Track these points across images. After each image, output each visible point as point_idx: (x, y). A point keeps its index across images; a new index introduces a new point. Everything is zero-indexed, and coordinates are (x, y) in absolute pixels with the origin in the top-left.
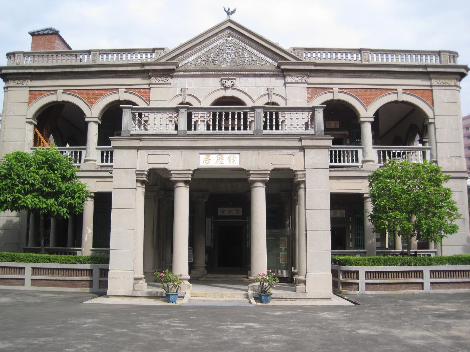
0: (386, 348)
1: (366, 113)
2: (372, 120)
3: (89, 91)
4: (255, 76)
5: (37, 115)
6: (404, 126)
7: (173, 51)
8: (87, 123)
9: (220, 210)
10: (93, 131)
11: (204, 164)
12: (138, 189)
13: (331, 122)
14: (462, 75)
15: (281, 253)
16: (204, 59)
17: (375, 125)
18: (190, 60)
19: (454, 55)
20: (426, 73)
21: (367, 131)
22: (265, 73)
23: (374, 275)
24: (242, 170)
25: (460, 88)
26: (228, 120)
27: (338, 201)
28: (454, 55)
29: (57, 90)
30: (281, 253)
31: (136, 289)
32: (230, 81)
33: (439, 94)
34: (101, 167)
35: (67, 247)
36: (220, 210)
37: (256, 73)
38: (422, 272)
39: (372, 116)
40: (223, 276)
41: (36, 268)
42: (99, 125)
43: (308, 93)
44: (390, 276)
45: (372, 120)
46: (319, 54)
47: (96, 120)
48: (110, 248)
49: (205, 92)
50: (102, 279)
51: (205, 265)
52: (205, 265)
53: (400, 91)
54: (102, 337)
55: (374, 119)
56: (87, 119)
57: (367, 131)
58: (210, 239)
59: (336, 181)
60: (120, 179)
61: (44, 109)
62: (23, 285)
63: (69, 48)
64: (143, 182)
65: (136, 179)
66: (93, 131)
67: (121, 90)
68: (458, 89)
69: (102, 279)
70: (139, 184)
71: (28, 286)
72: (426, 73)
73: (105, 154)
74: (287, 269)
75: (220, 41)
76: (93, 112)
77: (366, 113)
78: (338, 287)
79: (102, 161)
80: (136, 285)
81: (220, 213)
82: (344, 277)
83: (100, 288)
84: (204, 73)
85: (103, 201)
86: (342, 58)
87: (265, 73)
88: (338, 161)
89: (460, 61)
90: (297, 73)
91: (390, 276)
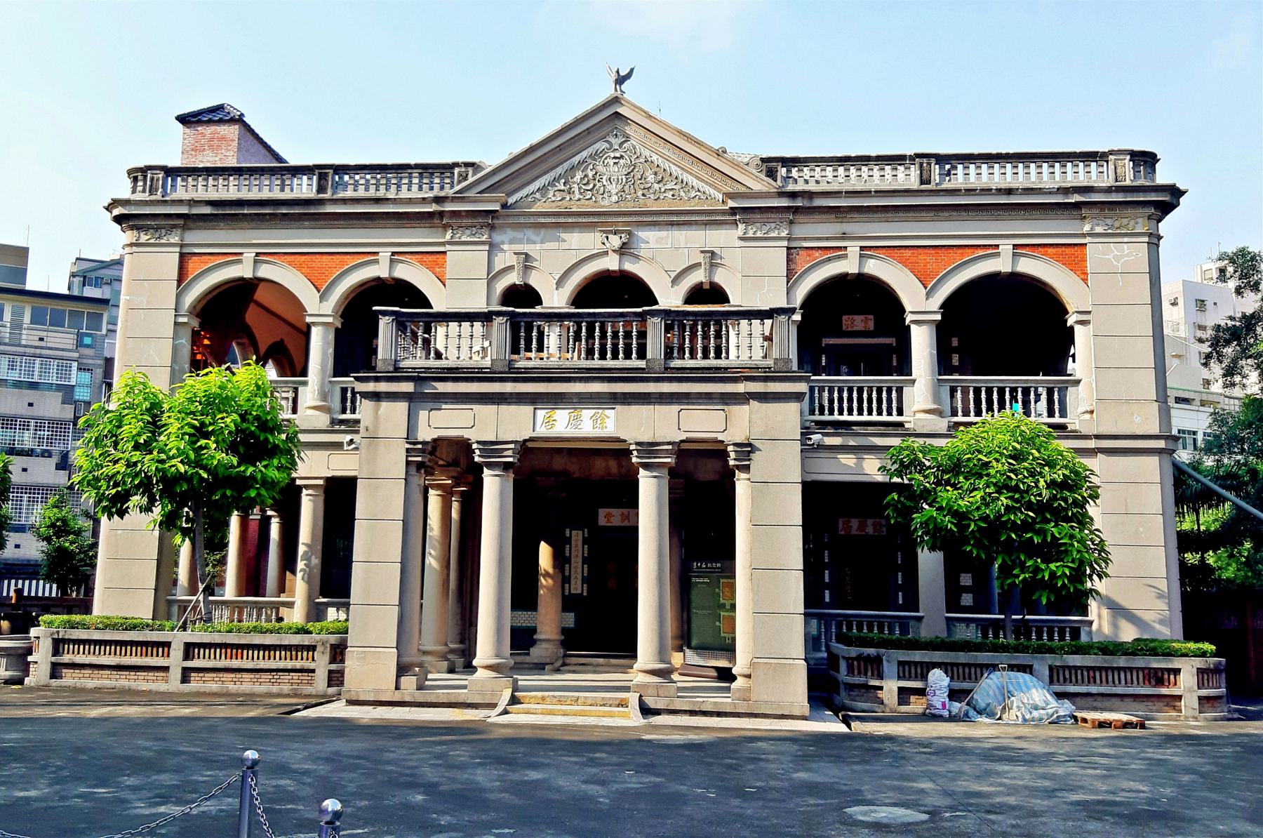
0: (73, 626)
1: (921, 302)
2: (939, 317)
3: (314, 257)
5: (199, 308)
9: (602, 512)
10: (320, 348)
13: (855, 317)
14: (1165, 208)
17: (943, 332)
21: (922, 344)
27: (823, 503)
28: (1146, 160)
29: (241, 254)
35: (944, 364)
36: (602, 512)
38: (622, 644)
39: (936, 309)
41: (909, 663)
45: (939, 317)
47: (330, 320)
48: (348, 596)
49: (557, 269)
50: (334, 667)
57: (922, 344)
58: (580, 577)
60: (367, 449)
61: (211, 296)
66: (320, 348)
71: (173, 682)
81: (602, 521)
83: (329, 686)
84: (562, 220)
85: (340, 495)
86: (877, 179)
89: (1163, 176)
90: (765, 216)
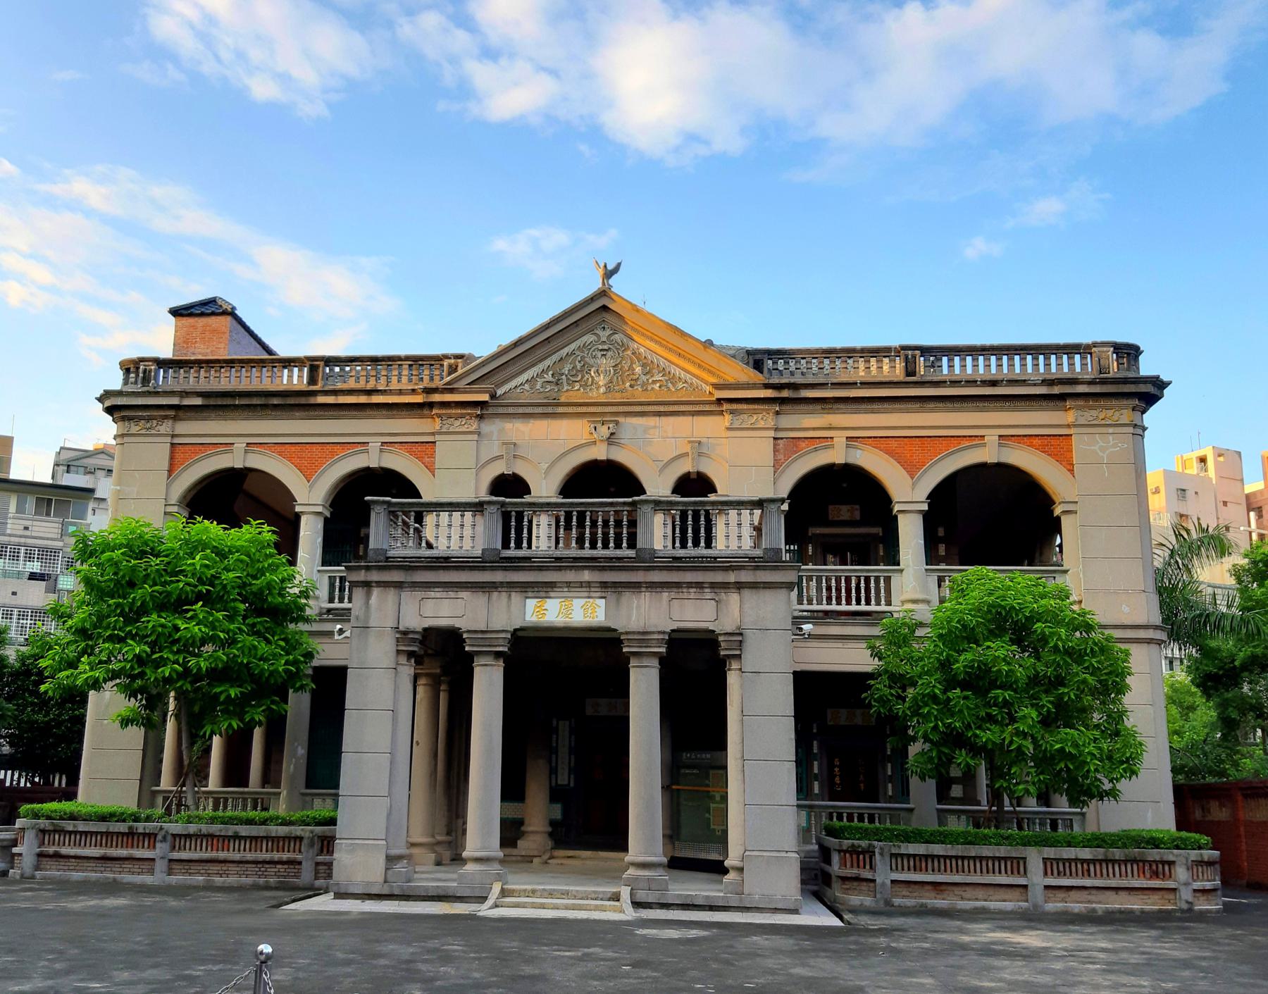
1: (909, 493)
2: (925, 507)
4: (659, 414)
6: (998, 517)
7: (484, 364)
8: (297, 517)
11: (534, 619)
12: (400, 668)
15: (712, 805)
16: (549, 377)
17: (931, 521)
18: (517, 385)
19: (1129, 352)
20: (1058, 394)
21: (911, 534)
22: (682, 408)
23: (912, 863)
24: (609, 630)
25: (1144, 429)
26: (584, 527)
28: (1129, 352)
30: (712, 805)
31: (389, 879)
32: (605, 427)
33: (1086, 446)
34: (329, 611)
37: (662, 409)
40: (588, 853)
42: (326, 519)
43: (775, 451)
44: (1105, 871)
46: (803, 362)
47: (320, 509)
49: (547, 452)
50: (321, 858)
51: (550, 829)
52: (550, 829)
53: (990, 439)
54: (310, 964)
55: (929, 505)
56: (298, 509)
57: (911, 534)
59: (840, 645)
62: (151, 872)
63: (269, 351)
64: (410, 655)
65: (394, 649)
67: (374, 445)
68: (1140, 432)
69: (321, 858)
70: (403, 659)
72: (1058, 394)
73: (337, 584)
74: (697, 844)
75: (585, 339)
76: (311, 496)
77: (909, 493)
78: (817, 881)
79: (331, 600)
80: (390, 872)
82: (843, 864)
85: (331, 685)
87: (682, 408)
88: (844, 602)
91: (1105, 871)
